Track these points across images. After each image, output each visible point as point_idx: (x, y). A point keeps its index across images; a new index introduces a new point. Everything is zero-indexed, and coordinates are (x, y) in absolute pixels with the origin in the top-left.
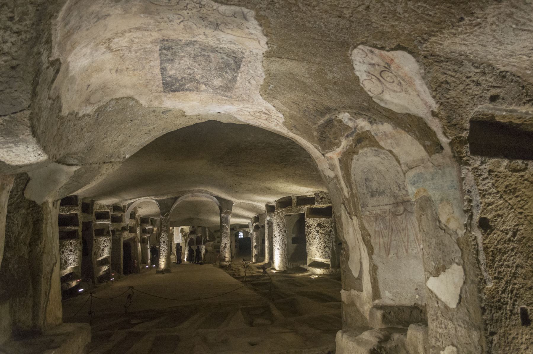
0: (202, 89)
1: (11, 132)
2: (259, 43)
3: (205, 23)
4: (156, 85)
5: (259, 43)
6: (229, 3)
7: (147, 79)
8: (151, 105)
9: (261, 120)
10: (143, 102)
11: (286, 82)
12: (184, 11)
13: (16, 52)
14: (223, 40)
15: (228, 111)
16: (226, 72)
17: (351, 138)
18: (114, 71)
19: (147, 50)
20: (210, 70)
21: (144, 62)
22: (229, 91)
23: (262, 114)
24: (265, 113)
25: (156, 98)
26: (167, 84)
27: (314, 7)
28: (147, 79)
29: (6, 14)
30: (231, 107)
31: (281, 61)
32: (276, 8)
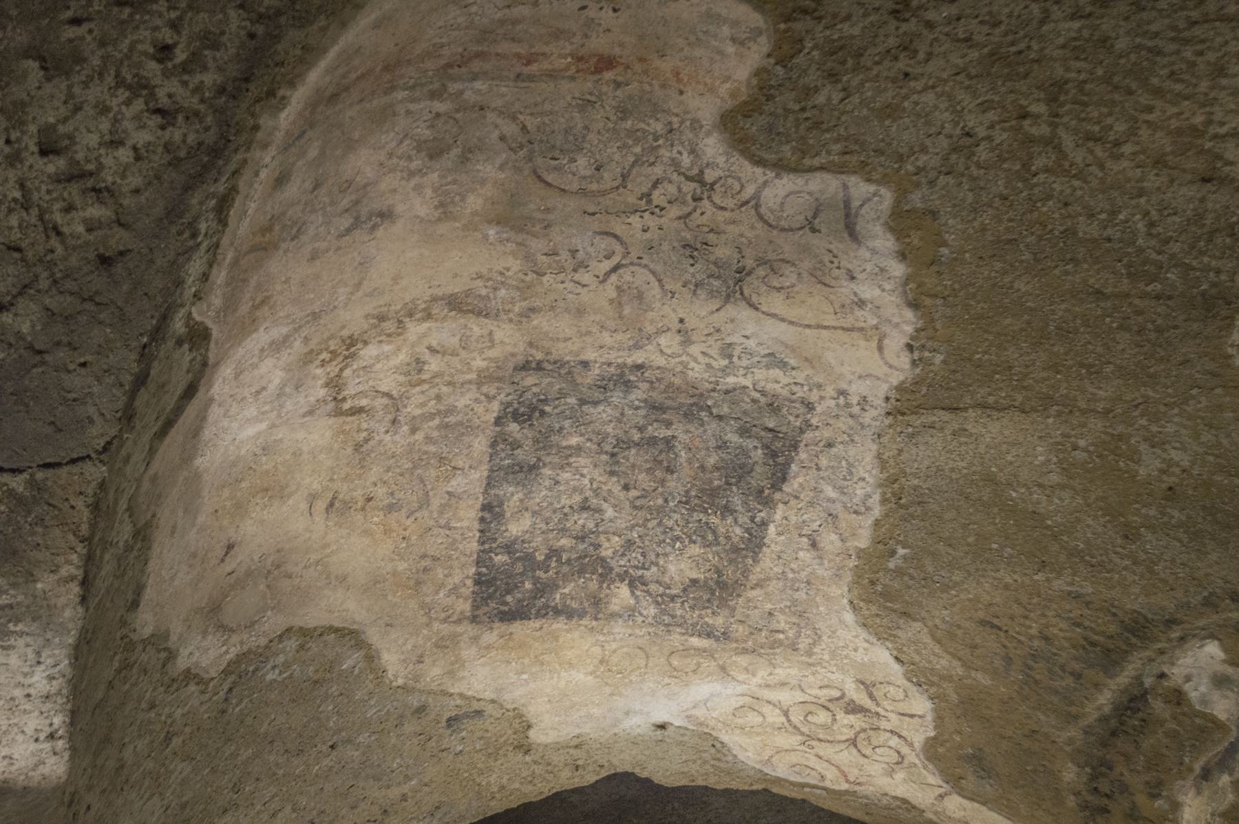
0: (615, 605)
1: (14, 553)
2: (880, 348)
3: (697, 271)
4: (451, 582)
5: (880, 348)
6: (807, 162)
7: (424, 556)
8: (416, 679)
9: (827, 751)
10: (392, 661)
11: (965, 527)
12: (635, 220)
13: (137, 191)
14: (746, 351)
15: (700, 713)
16: (727, 510)
17: (1225, 779)
18: (321, 505)
19: (452, 419)
20: (660, 511)
21: (433, 473)
22: (723, 603)
23: (840, 716)
24: (853, 708)
25: (442, 645)
26: (490, 583)
27: (1117, 144)
28: (424, 556)
29: (156, 29)
30: (717, 687)
31: (952, 422)
32: (979, 166)
